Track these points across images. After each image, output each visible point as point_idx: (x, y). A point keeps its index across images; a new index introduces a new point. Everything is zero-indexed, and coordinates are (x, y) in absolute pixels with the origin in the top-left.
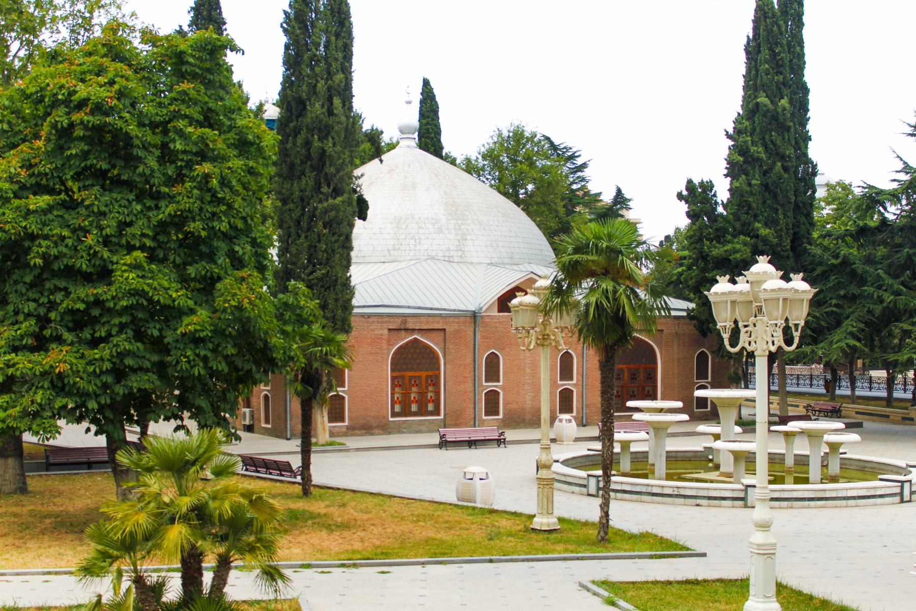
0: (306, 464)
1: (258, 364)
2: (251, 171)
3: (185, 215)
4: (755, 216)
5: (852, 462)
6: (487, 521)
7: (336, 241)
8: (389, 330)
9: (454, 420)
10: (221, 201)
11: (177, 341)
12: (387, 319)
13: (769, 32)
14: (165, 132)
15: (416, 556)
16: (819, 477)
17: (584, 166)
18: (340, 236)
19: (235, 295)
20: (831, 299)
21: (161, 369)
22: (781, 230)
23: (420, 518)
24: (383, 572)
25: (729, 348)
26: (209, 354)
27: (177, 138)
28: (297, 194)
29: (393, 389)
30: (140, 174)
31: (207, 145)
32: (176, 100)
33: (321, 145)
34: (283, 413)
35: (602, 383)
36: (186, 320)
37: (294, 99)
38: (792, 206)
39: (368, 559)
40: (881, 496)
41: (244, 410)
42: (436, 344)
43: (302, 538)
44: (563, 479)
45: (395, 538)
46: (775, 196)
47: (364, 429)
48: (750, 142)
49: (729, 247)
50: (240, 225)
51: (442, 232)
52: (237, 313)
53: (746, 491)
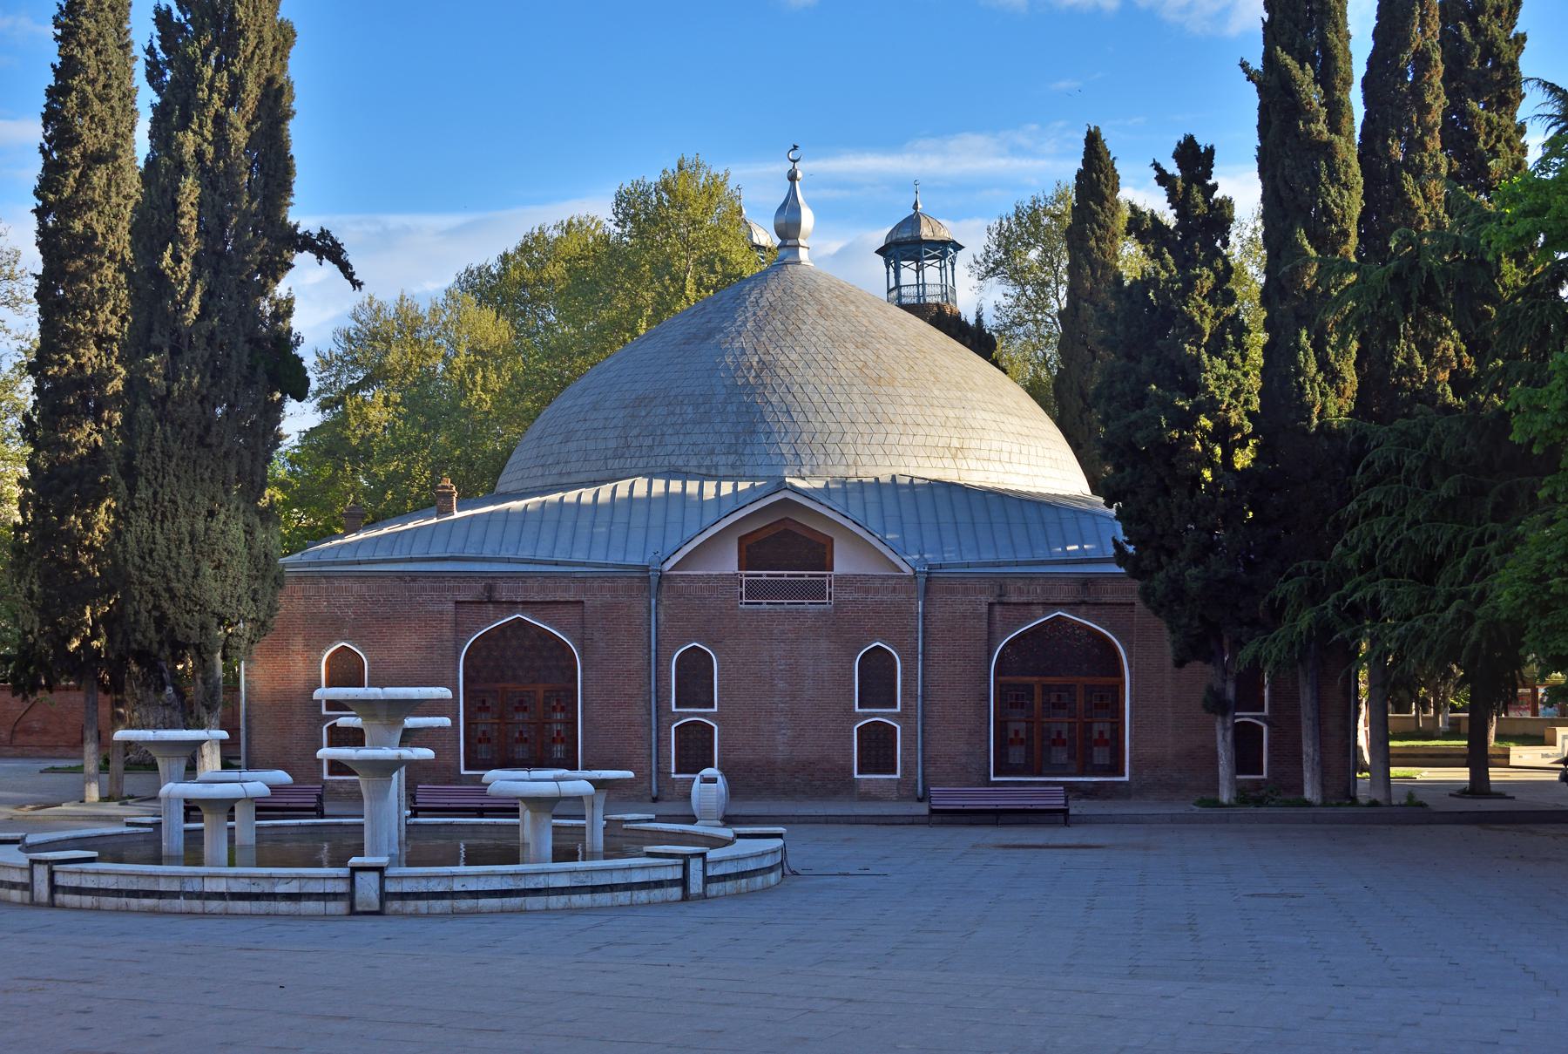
5: (113, 840)
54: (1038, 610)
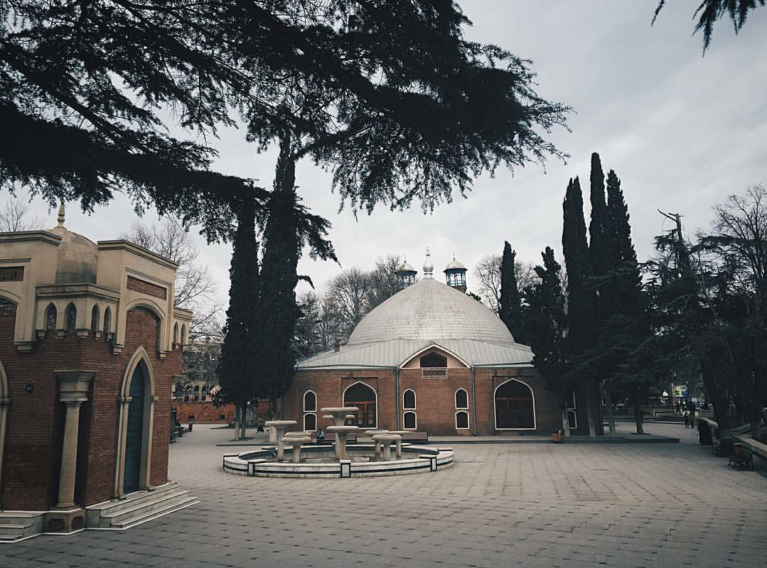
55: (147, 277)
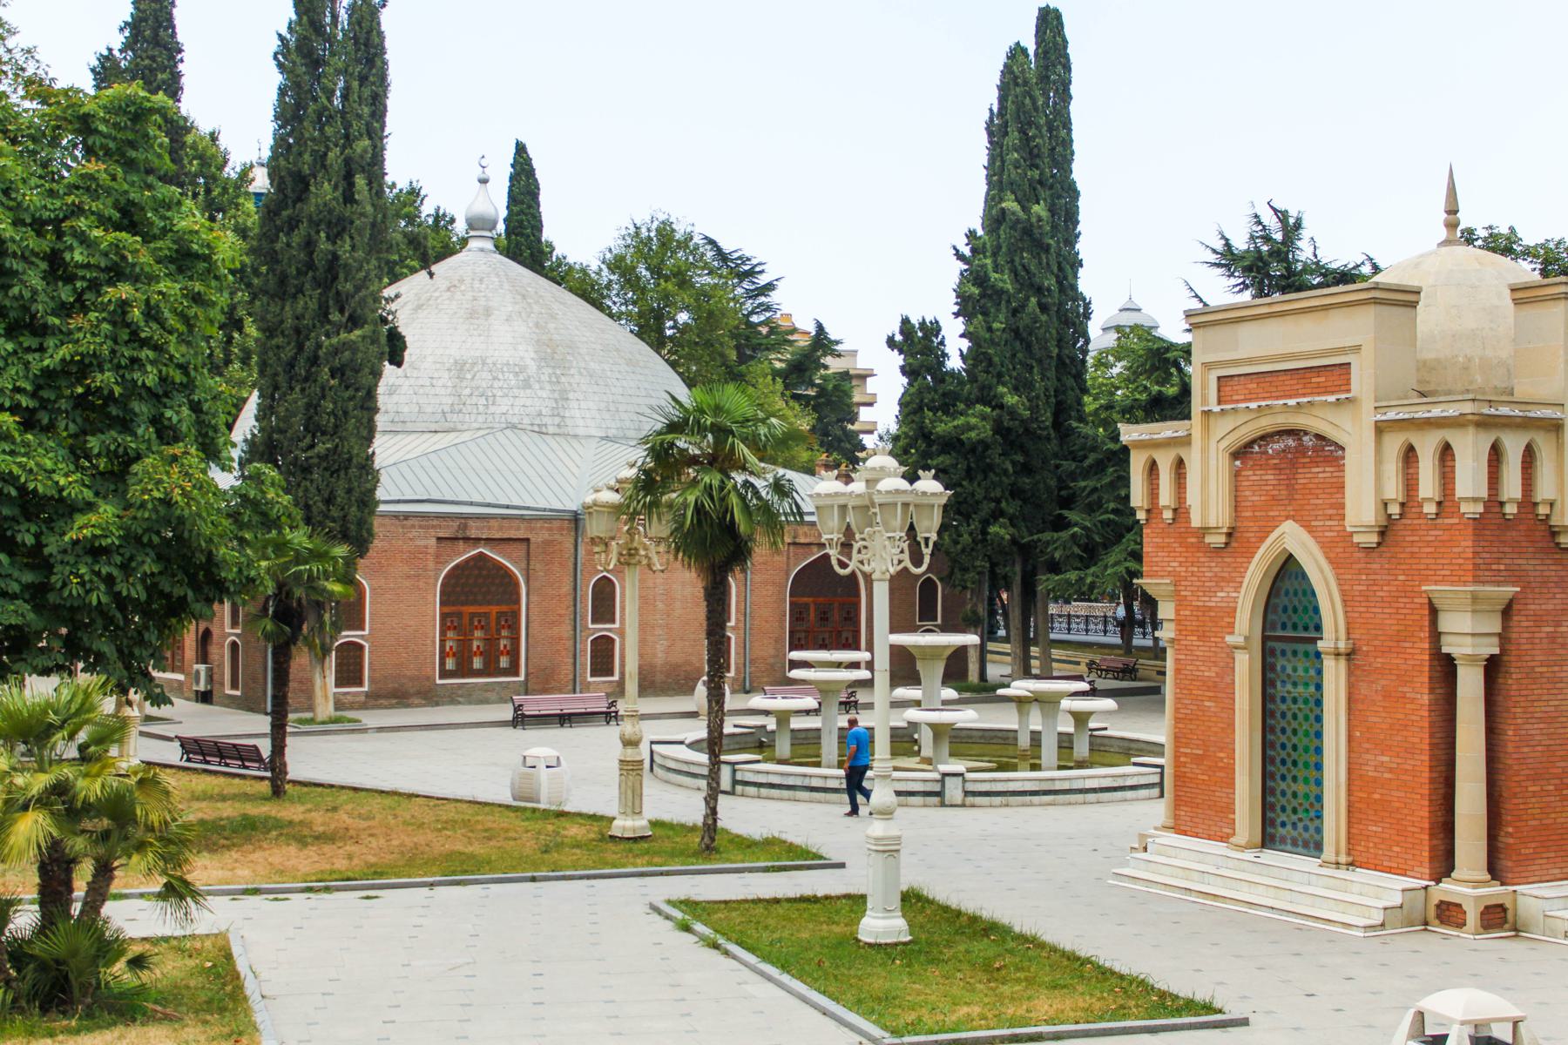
0: (279, 748)
1: (197, 588)
2: (197, 299)
3: (87, 361)
4: (1000, 375)
6: (550, 828)
7: (351, 398)
8: (439, 539)
9: (542, 682)
10: (144, 343)
11: (65, 551)
12: (435, 522)
13: (1020, 106)
14: (60, 235)
15: (425, 875)
16: (1055, 763)
17: (770, 287)
18: (357, 390)
19: (160, 482)
20: (1108, 501)
21: (37, 594)
22: (1038, 397)
23: (450, 824)
24: (368, 898)
25: (837, 568)
26: (115, 572)
27: (75, 244)
28: (289, 322)
29: (443, 633)
30: (15, 298)
31: (124, 258)
32: (77, 188)
33: (330, 247)
34: (260, 670)
35: (708, 619)
36: (80, 520)
37: (290, 173)
38: (1054, 363)
39: (348, 879)
40: (1133, 788)
41: (196, 666)
42: (515, 563)
43: (258, 855)
44: (685, 768)
45: (402, 853)
46: (1029, 347)
47: (396, 697)
48: (990, 267)
49: (961, 421)
50: (178, 377)
51: (530, 387)
52: (162, 510)
53: (942, 782)
54: (815, 549)
55: (1250, 361)
